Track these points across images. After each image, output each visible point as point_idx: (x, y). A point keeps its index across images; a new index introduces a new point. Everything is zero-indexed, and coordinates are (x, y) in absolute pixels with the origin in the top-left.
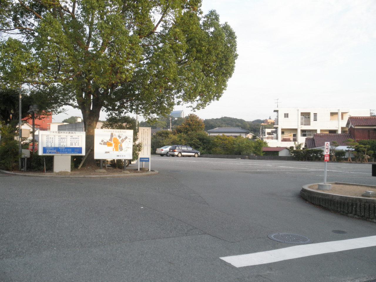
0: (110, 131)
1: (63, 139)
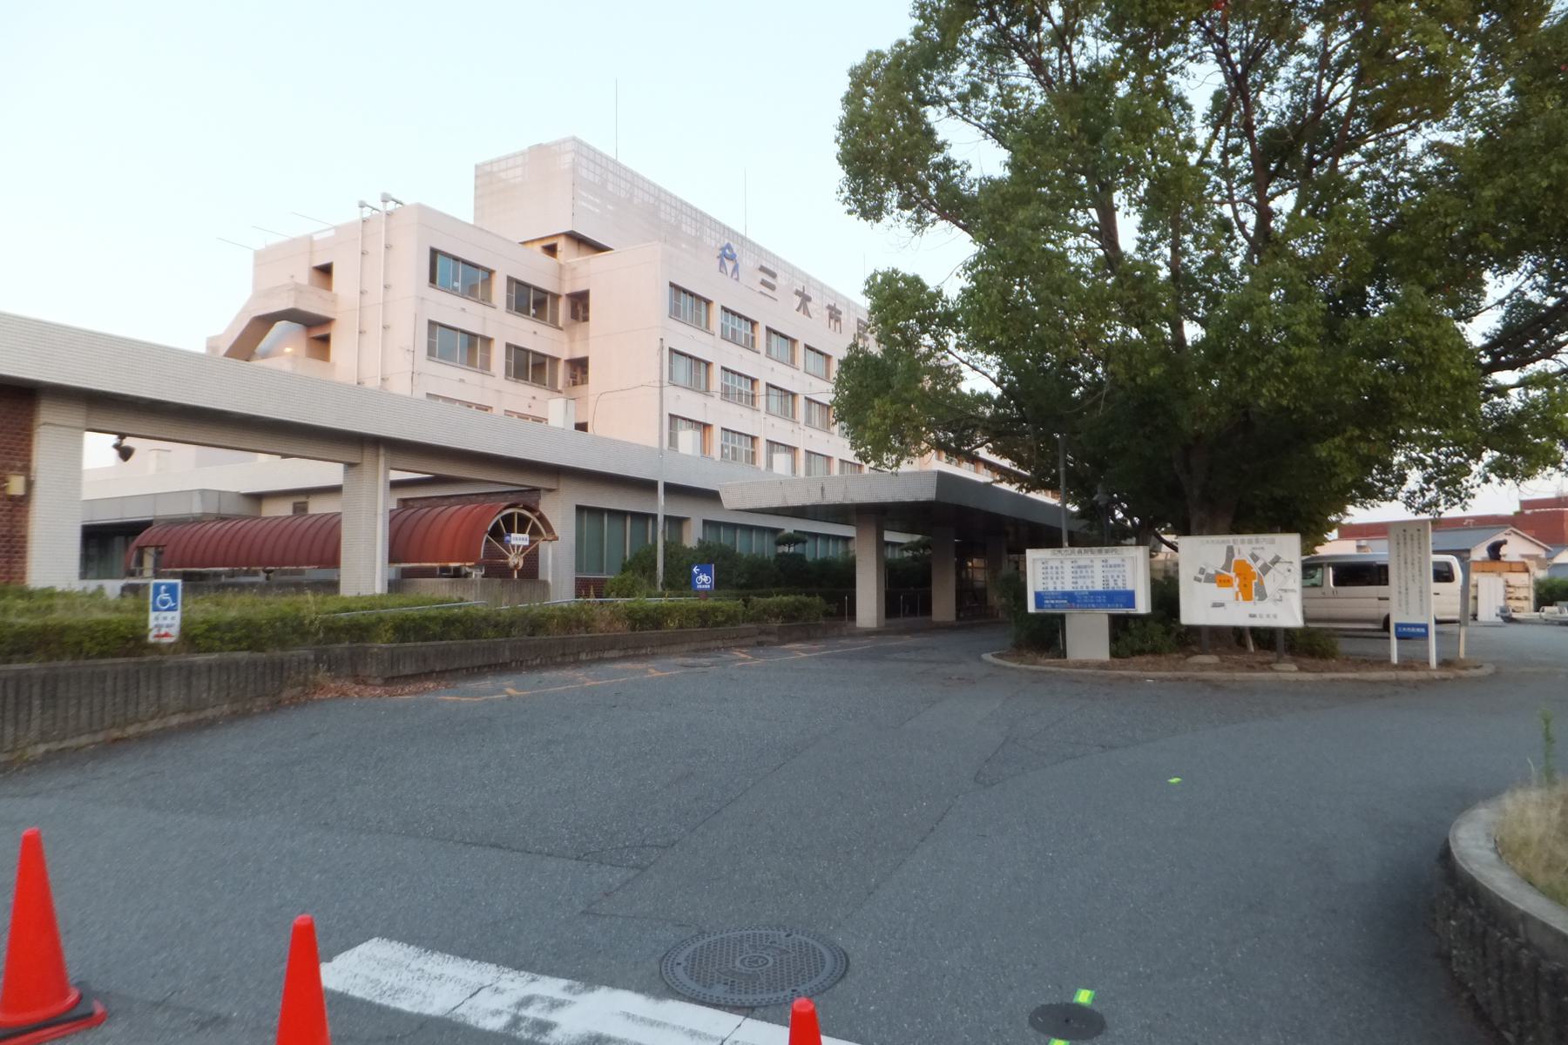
0: (1223, 542)
1: (1084, 570)
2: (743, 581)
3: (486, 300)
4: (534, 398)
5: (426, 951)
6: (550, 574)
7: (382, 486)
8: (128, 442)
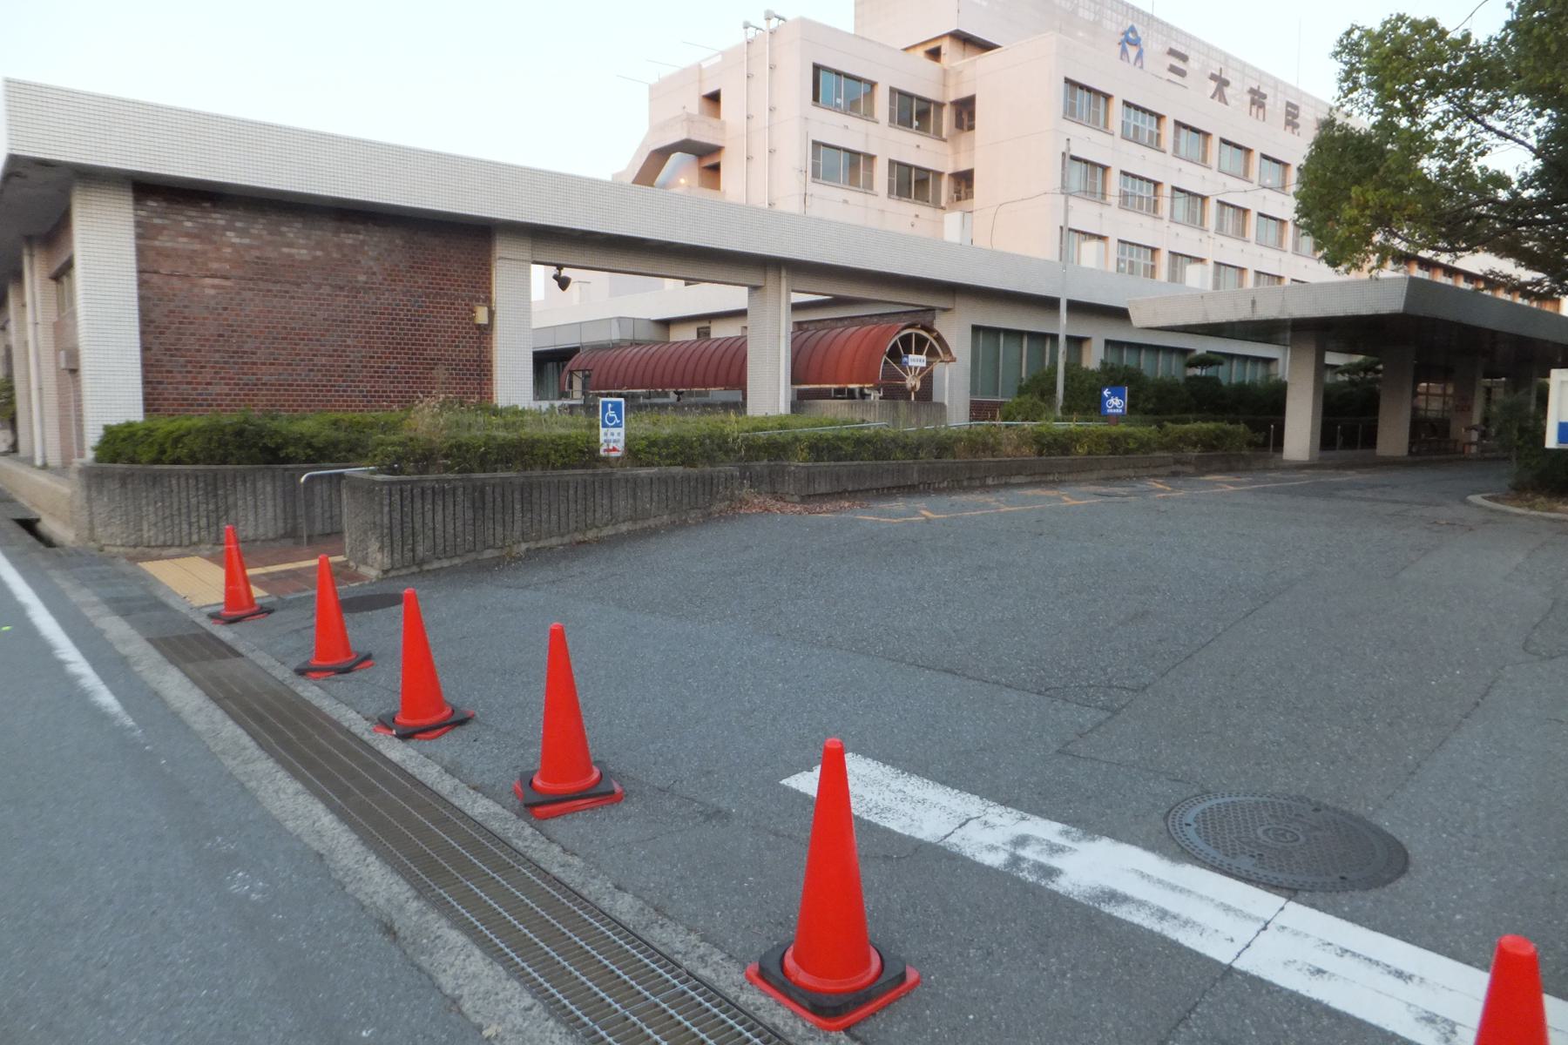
2: (1150, 406)
3: (869, 115)
4: (917, 216)
5: (903, 773)
6: (947, 393)
7: (785, 309)
8: (566, 272)
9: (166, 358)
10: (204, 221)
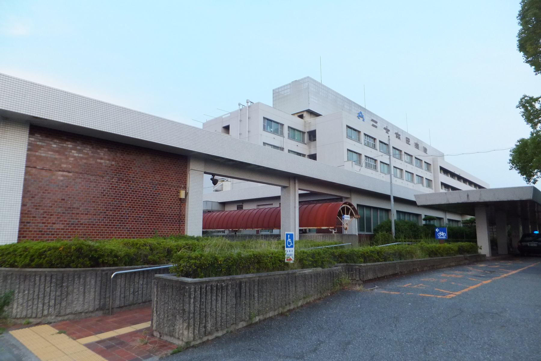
3: (282, 134)
8: (216, 177)
9: (33, 210)
10: (62, 145)
